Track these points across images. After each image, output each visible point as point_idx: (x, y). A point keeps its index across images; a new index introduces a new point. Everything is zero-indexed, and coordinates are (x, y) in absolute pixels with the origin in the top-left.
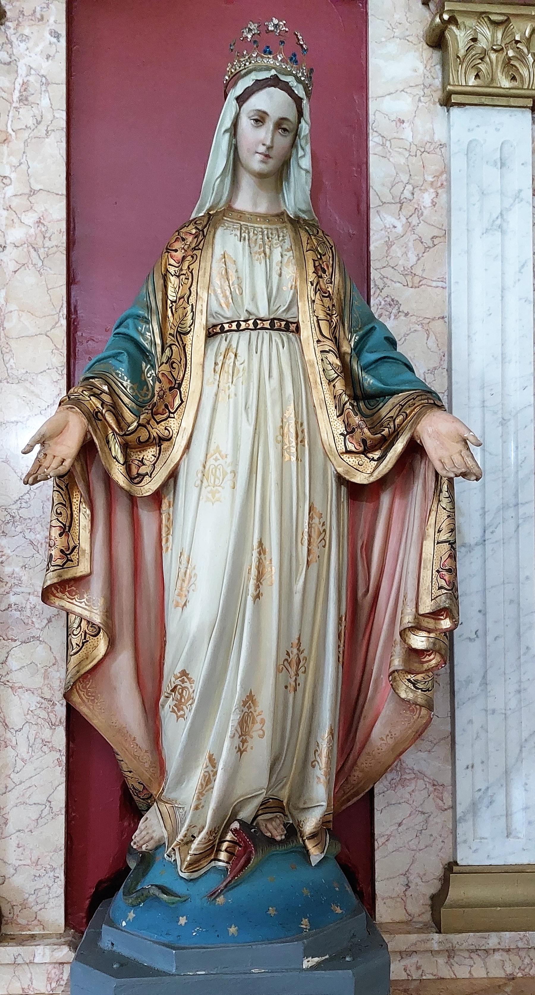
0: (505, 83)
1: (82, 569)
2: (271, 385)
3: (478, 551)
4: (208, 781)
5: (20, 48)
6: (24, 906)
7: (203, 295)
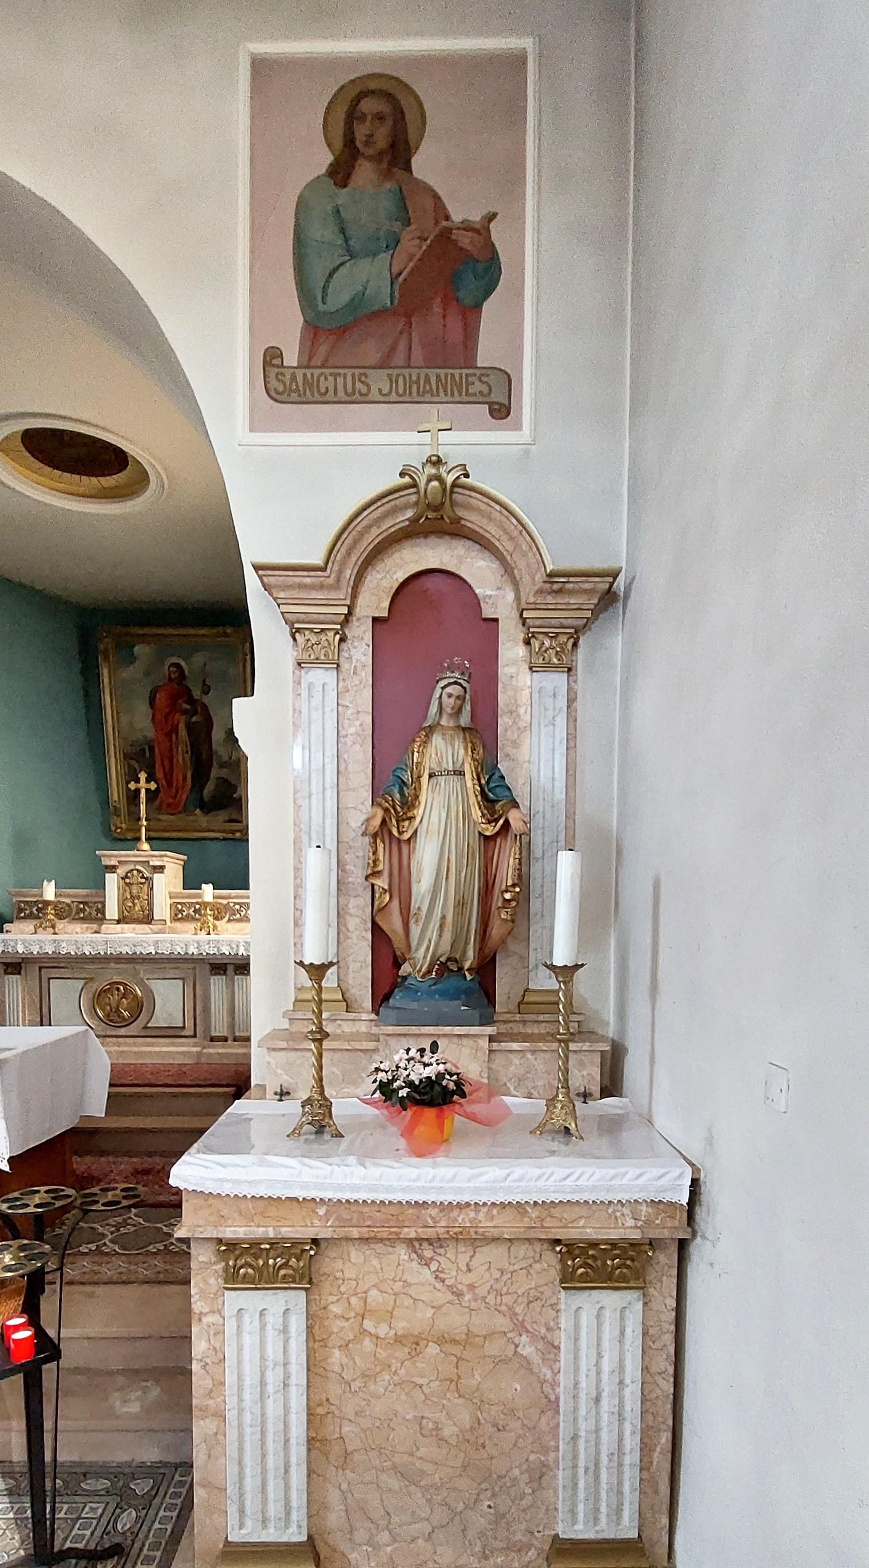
0: (555, 661)
1: (380, 868)
2: (453, 798)
3: (541, 860)
4: (428, 948)
5: (353, 651)
6: (356, 1001)
7: (428, 762)
